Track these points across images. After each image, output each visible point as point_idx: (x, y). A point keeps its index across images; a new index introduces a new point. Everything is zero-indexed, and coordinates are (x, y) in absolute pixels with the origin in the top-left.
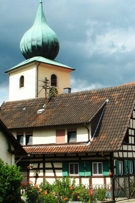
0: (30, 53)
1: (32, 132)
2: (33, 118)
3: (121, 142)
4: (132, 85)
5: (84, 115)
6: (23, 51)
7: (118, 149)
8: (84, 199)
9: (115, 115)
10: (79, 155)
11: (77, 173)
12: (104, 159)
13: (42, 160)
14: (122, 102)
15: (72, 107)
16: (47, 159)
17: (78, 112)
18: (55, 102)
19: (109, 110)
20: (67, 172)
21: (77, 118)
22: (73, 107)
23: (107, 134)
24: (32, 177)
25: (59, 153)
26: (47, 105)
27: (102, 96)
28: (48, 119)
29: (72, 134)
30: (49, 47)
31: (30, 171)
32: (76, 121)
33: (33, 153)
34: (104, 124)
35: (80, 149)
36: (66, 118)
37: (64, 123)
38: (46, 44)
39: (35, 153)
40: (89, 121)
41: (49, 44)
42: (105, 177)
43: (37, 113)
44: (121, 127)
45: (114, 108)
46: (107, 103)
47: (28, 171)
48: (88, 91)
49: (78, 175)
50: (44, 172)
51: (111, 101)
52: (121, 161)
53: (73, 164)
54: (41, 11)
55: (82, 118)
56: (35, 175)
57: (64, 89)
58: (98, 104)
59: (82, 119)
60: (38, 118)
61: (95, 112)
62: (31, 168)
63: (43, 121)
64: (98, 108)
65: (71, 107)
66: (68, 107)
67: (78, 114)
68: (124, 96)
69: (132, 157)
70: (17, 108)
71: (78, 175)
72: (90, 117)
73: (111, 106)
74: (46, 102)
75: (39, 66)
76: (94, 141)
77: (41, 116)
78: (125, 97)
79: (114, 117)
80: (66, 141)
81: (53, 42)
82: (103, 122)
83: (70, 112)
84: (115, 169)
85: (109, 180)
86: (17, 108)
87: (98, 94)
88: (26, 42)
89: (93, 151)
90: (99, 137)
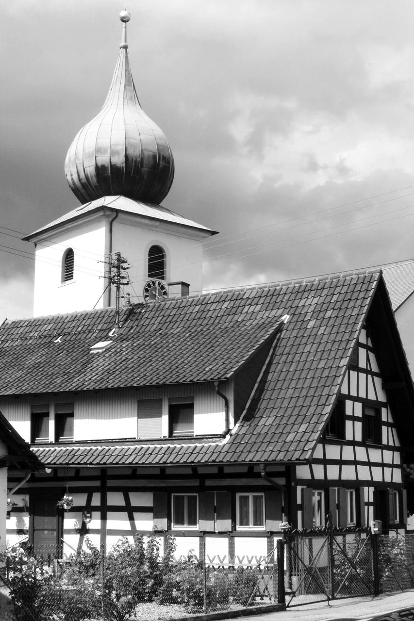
1: (72, 405)
3: (316, 436)
6: (72, 179)
7: (307, 457)
10: (201, 471)
11: (193, 522)
12: (269, 484)
13: (97, 483)
14: (325, 322)
15: (188, 335)
16: (110, 482)
18: (141, 323)
19: (288, 345)
20: (166, 520)
21: (197, 368)
22: (190, 335)
24: (69, 532)
25: (144, 466)
26: (122, 331)
27: (271, 305)
28: (118, 368)
29: (180, 413)
30: (145, 169)
31: (66, 514)
33: (91, 463)
34: (272, 383)
35: (210, 455)
36: (167, 368)
37: (158, 381)
38: (136, 161)
39: (79, 463)
40: (228, 376)
41: (145, 162)
42: (270, 534)
43: (91, 352)
44: (318, 393)
45: (304, 341)
46: (285, 327)
47: (60, 514)
50: (104, 518)
51: (295, 319)
53: (183, 497)
54: (124, 71)
55: (211, 367)
58: (259, 328)
60: (92, 366)
61: (247, 349)
63: (103, 374)
64: (257, 339)
66: (176, 336)
67: (201, 356)
68: (332, 306)
69: (355, 479)
70: (40, 337)
72: (231, 365)
73: (295, 333)
74: (119, 321)
75: (114, 224)
77: (101, 360)
78: (336, 308)
79: (301, 364)
80: (165, 433)
81: (154, 157)
83: (181, 349)
84: (299, 513)
86: (40, 337)
87: (262, 300)
88: (81, 156)
89: (235, 461)
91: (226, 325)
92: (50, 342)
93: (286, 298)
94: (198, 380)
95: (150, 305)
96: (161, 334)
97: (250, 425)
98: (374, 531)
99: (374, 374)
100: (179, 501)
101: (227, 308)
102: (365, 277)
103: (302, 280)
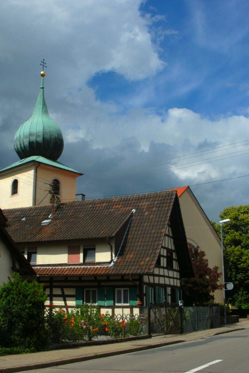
1: (36, 248)
4: (165, 192)
5: (104, 228)
9: (144, 228)
10: (99, 278)
14: (153, 213)
15: (88, 217)
17: (96, 225)
20: (81, 301)
22: (89, 218)
23: (135, 252)
27: (126, 205)
28: (57, 231)
32: (95, 235)
36: (82, 232)
38: (48, 140)
40: (113, 235)
45: (144, 221)
50: (51, 300)
51: (138, 211)
54: (42, 99)
57: (76, 195)
60: (44, 230)
63: (50, 234)
65: (86, 218)
66: (82, 218)
70: (14, 218)
71: (97, 304)
72: (113, 231)
73: (139, 217)
74: (53, 211)
76: (118, 261)
77: (48, 228)
80: (81, 261)
84: (145, 297)
85: (136, 311)
87: (121, 203)
88: (22, 137)
90: (125, 256)
91: (105, 213)
92: (20, 220)
93: (133, 202)
94: (98, 237)
95: (67, 204)
96: (74, 217)
97: (122, 258)
98: (181, 305)
99: (171, 237)
100: (88, 292)
101: (105, 206)
102: (169, 193)
103: (139, 194)
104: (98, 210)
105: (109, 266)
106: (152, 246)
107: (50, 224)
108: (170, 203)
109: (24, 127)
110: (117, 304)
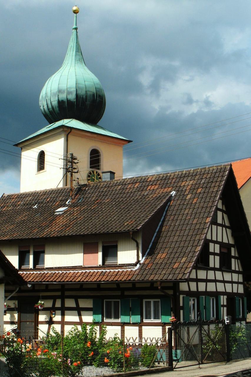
0: (55, 113)
1: (43, 246)
2: (48, 223)
3: (192, 264)
4: (215, 167)
5: (131, 218)
6: (44, 109)
7: (186, 278)
8: (115, 363)
9: (184, 217)
10: (122, 286)
11: (117, 317)
13: (59, 293)
14: (197, 195)
15: (114, 203)
16: (67, 292)
18: (86, 196)
20: (100, 316)
22: (115, 203)
25: (87, 283)
26: (74, 201)
27: (164, 185)
28: (71, 223)
29: (110, 252)
30: (88, 103)
31: (40, 312)
32: (116, 228)
33: (44, 281)
34: (165, 233)
36: (101, 223)
38: (82, 97)
40: (138, 228)
41: (88, 98)
43: (56, 213)
44: (193, 239)
45: (184, 207)
47: (37, 313)
48: (143, 177)
49: (119, 321)
50: (63, 315)
51: (179, 194)
52: (240, 297)
53: (111, 302)
55: (128, 223)
56: (47, 320)
58: (157, 199)
59: (128, 224)
60: (56, 222)
62: (41, 307)
63: (62, 227)
66: (106, 204)
68: (201, 186)
70: (24, 205)
71: (119, 321)
73: (179, 202)
74: (72, 195)
77: (61, 219)
78: (204, 187)
79: (183, 221)
80: (100, 263)
81: (94, 95)
82: (163, 230)
83: (109, 212)
84: (182, 311)
86: (24, 205)
87: (159, 182)
88: (49, 95)
89: (143, 280)
90: (155, 255)
91: (137, 197)
92: (30, 207)
96: (97, 203)
97: (152, 258)
98: (227, 323)
99: (226, 227)
100: (109, 304)
102: (221, 168)
104: (128, 193)
105: (134, 270)
106: (191, 242)
107: (65, 213)
108: (221, 181)
109: (50, 82)
110: (145, 321)
